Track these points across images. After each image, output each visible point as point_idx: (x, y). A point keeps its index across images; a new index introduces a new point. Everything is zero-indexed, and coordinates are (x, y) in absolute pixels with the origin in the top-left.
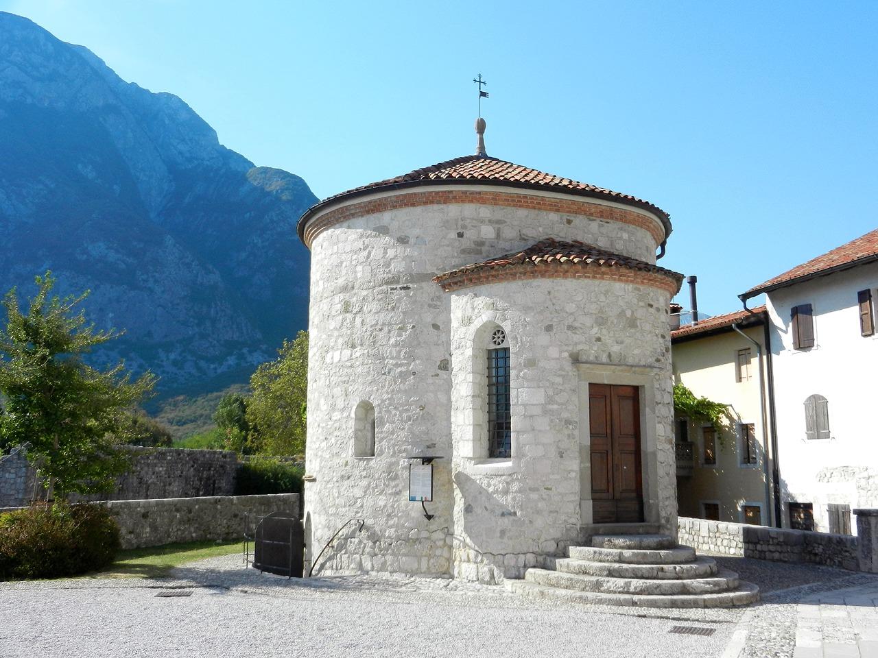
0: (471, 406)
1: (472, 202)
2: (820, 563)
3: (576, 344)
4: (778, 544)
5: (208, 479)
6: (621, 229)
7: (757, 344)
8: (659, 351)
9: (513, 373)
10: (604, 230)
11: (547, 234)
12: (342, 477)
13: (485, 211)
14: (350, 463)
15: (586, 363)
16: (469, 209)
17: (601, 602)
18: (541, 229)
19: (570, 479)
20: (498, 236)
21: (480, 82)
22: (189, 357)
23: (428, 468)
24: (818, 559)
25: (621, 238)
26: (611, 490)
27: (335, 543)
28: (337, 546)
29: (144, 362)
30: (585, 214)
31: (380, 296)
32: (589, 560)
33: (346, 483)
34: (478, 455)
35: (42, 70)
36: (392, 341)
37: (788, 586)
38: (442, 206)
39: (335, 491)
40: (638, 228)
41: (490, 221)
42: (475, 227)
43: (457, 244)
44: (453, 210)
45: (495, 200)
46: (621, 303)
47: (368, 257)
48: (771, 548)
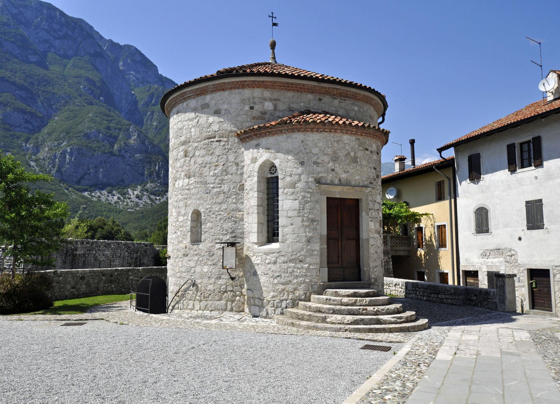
0: (256, 211)
1: (259, 87)
2: (475, 305)
3: (319, 173)
4: (450, 294)
5: (136, 258)
6: (353, 104)
7: (448, 178)
8: (372, 177)
9: (280, 191)
10: (342, 105)
11: (306, 107)
12: (184, 255)
13: (267, 94)
14: (188, 247)
15: (325, 184)
16: (257, 92)
17: (326, 329)
18: (302, 104)
19: (314, 255)
20: (275, 108)
21: (272, 17)
22: (145, 193)
23: (233, 249)
24: (473, 303)
25: (353, 110)
26: (340, 261)
27: (180, 294)
28: (181, 294)
29: (120, 196)
30: (330, 94)
31: (204, 146)
32: (323, 303)
33: (186, 258)
34: (260, 242)
35: (59, 33)
36: (211, 173)
37: (450, 320)
38: (240, 90)
39: (180, 263)
40: (365, 104)
41: (270, 99)
42: (261, 103)
43: (250, 113)
44: (247, 93)
45: (273, 86)
46: (348, 147)
47: (198, 123)
48: (447, 296)
